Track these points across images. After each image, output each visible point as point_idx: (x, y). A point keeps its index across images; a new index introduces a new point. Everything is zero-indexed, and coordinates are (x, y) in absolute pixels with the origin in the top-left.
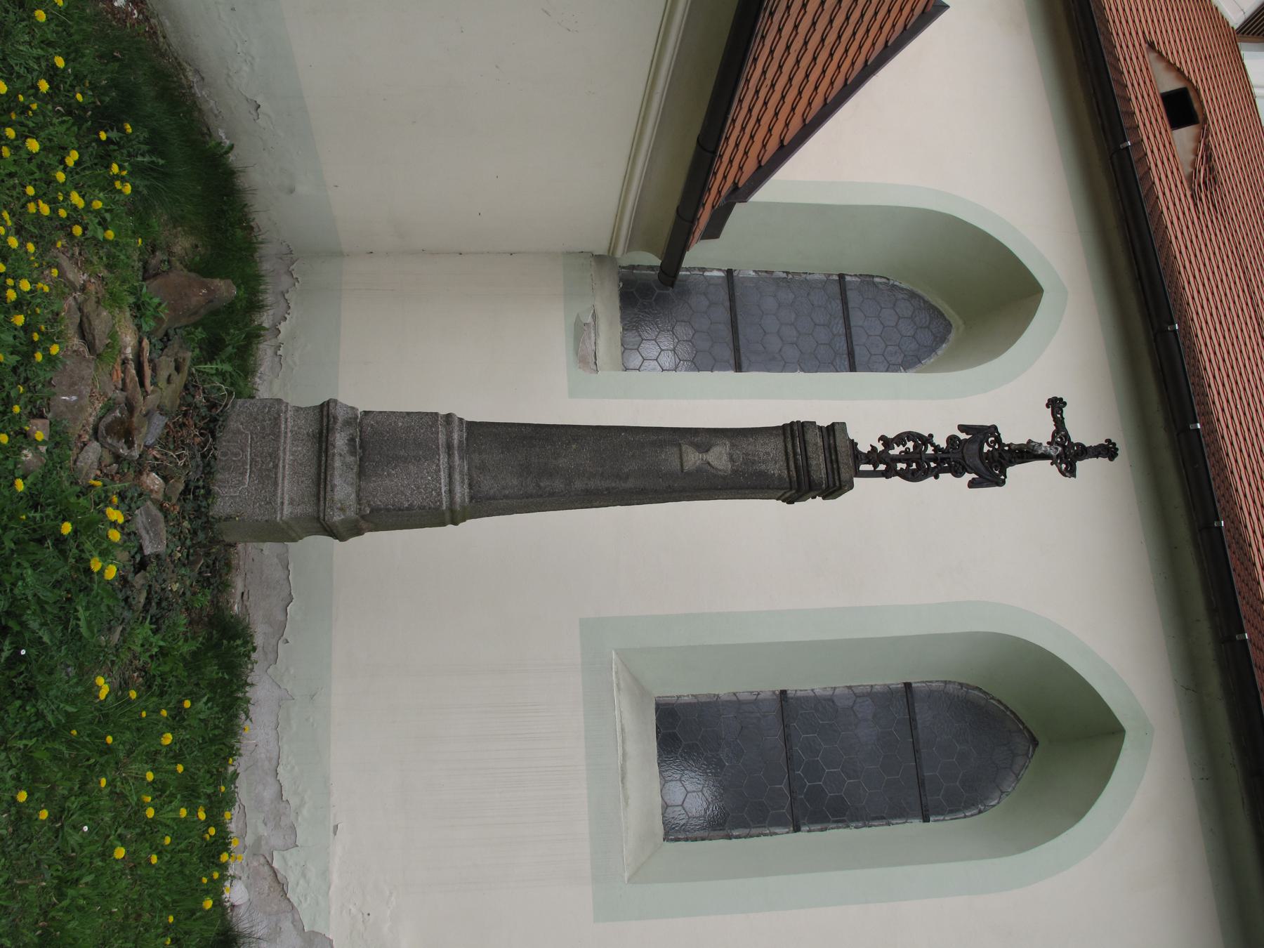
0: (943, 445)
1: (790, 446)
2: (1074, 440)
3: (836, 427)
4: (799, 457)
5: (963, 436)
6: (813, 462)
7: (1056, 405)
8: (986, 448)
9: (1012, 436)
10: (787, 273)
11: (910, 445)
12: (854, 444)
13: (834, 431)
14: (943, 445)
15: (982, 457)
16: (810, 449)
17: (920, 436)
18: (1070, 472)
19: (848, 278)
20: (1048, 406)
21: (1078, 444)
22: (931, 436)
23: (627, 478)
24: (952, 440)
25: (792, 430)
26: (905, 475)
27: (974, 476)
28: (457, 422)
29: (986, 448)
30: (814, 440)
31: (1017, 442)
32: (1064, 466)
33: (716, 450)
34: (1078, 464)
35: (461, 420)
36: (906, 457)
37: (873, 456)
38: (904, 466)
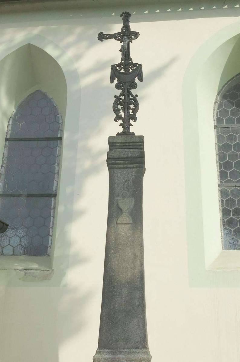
0: (120, 91)
1: (120, 166)
2: (120, 31)
3: (111, 141)
4: (126, 162)
5: (116, 81)
6: (130, 155)
7: (102, 37)
8: (123, 71)
9: (118, 58)
10: (2, 166)
11: (120, 107)
12: (118, 134)
13: (112, 143)
14: (120, 91)
15: (127, 75)
16: (122, 156)
17: (115, 102)
18: (136, 34)
19: (8, 137)
20: (102, 41)
21: (122, 30)
22: (115, 96)
23: (135, 255)
24: (117, 87)
25: (112, 164)
26: (135, 111)
27: (137, 78)
28: (98, 355)
29: (123, 71)
30: (117, 153)
31: (121, 57)
32: (133, 37)
33: (121, 205)
34: (132, 30)
35: (97, 352)
36: (126, 109)
37: (126, 125)
38: (131, 111)
